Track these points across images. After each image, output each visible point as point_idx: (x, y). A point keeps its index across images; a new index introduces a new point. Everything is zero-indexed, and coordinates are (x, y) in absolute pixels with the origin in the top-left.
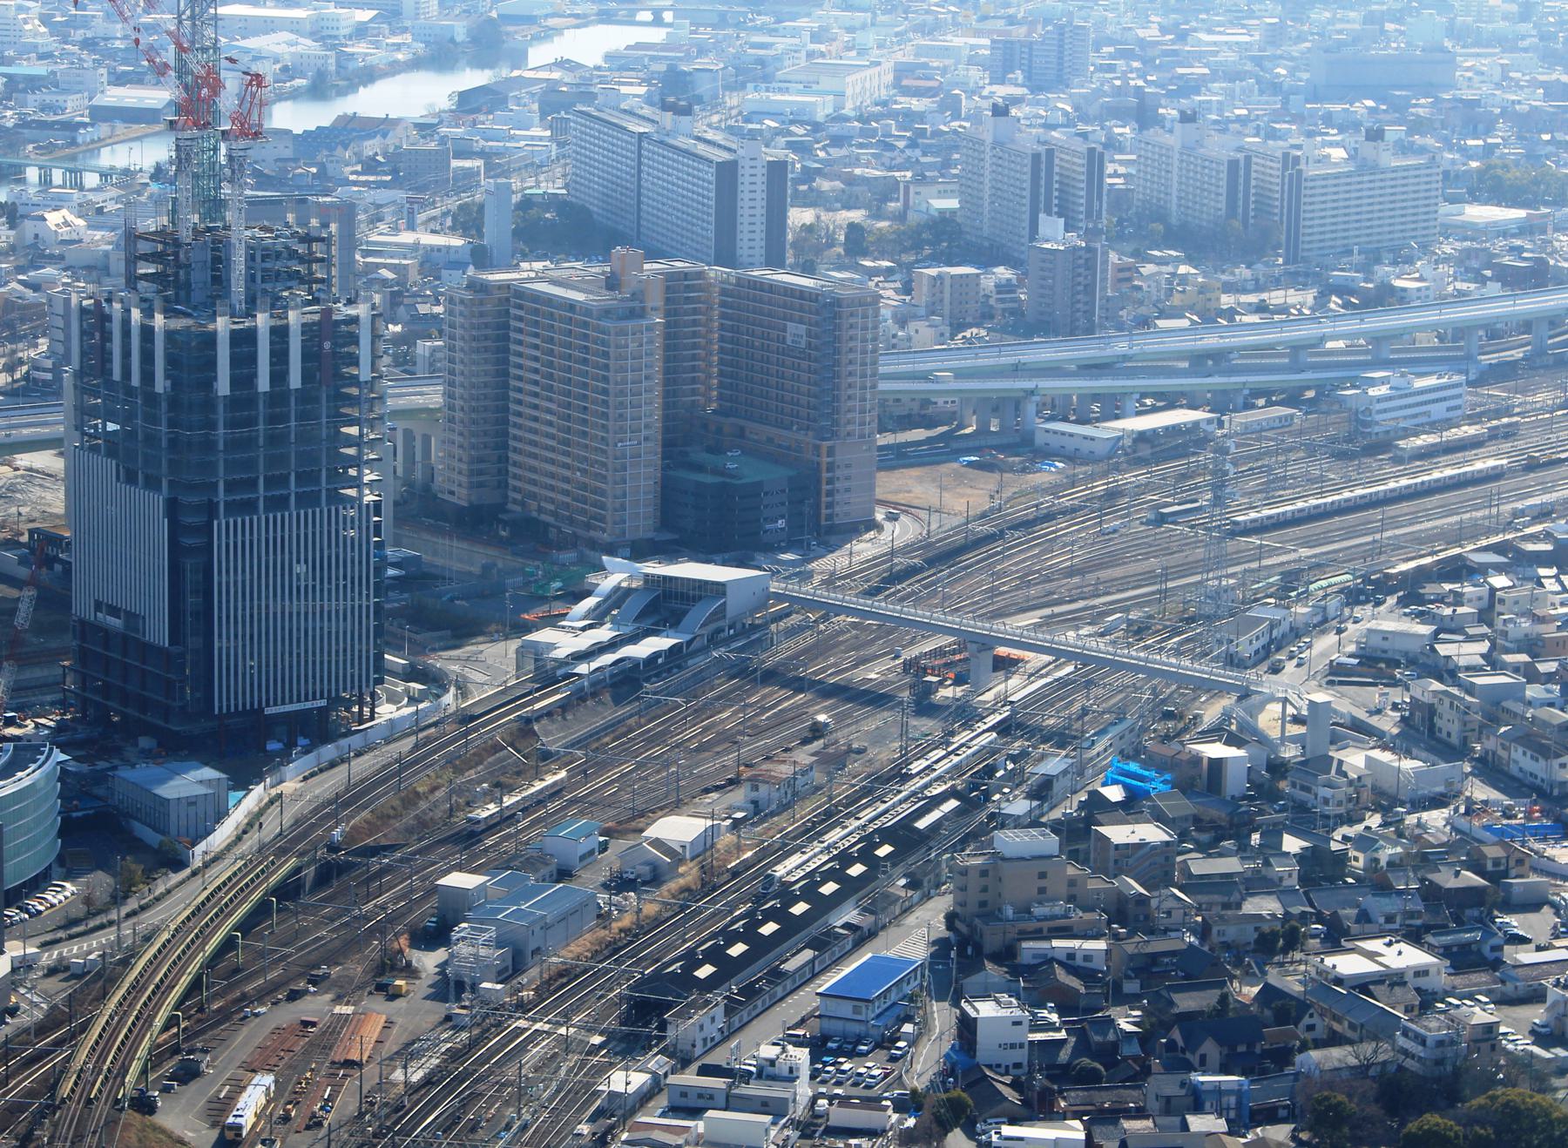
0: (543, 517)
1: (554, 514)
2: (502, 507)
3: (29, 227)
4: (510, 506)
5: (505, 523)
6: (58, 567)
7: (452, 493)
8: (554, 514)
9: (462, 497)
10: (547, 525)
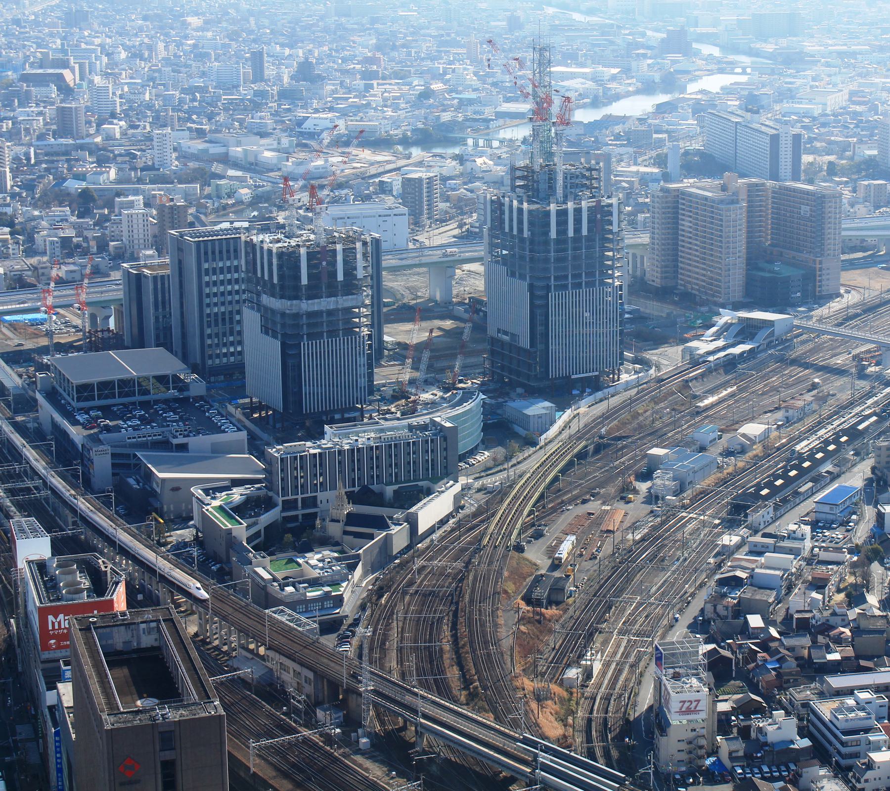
0: (694, 292)
1: (698, 290)
2: (675, 287)
3: (469, 165)
4: (679, 287)
5: (677, 294)
6: (481, 314)
7: (653, 281)
8: (698, 290)
9: (658, 283)
10: (695, 295)
